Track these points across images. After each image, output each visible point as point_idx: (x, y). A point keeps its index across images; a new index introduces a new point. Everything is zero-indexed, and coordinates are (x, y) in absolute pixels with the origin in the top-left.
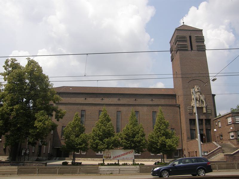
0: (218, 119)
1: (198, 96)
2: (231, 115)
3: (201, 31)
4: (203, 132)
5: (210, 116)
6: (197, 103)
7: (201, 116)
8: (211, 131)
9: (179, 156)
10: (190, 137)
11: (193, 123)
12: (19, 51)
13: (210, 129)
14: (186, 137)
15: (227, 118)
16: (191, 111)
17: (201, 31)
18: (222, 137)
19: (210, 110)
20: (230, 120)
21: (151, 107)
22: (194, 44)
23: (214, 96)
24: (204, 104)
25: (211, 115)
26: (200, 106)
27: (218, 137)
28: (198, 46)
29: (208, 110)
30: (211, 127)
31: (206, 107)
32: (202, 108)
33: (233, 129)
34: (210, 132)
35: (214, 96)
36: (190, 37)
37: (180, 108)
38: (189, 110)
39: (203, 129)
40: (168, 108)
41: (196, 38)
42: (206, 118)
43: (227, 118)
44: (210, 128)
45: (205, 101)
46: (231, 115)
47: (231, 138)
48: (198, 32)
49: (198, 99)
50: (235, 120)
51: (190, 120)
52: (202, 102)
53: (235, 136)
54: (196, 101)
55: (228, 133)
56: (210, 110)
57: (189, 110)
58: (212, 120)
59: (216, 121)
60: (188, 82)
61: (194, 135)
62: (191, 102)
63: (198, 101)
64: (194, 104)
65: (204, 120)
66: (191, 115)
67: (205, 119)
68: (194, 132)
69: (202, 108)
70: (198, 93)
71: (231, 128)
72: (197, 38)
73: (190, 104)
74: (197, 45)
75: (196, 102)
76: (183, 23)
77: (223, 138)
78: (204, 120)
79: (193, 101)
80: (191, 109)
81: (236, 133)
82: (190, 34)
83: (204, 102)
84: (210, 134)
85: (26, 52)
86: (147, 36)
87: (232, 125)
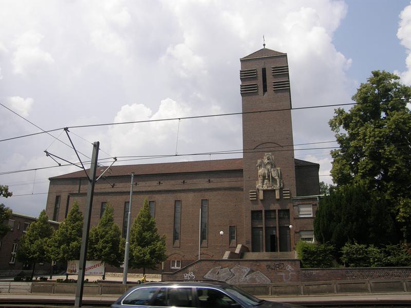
1: (266, 172)
3: (285, 56)
6: (265, 182)
7: (272, 205)
10: (251, 241)
12: (130, 105)
16: (288, 193)
17: (285, 56)
19: (289, 195)
21: (200, 193)
22: (270, 80)
26: (270, 188)
28: (277, 85)
32: (274, 191)
36: (264, 70)
38: (251, 195)
39: (276, 227)
40: (227, 192)
41: (273, 70)
42: (280, 209)
48: (278, 59)
50: (299, 212)
51: (253, 212)
52: (274, 180)
57: (251, 195)
63: (267, 179)
64: (259, 185)
65: (277, 211)
66: (255, 204)
68: (261, 232)
69: (274, 191)
72: (276, 69)
73: (255, 184)
74: (274, 83)
76: (264, 45)
78: (277, 211)
82: (264, 64)
83: (278, 181)
84: (288, 236)
85: (141, 104)
86: (340, 56)
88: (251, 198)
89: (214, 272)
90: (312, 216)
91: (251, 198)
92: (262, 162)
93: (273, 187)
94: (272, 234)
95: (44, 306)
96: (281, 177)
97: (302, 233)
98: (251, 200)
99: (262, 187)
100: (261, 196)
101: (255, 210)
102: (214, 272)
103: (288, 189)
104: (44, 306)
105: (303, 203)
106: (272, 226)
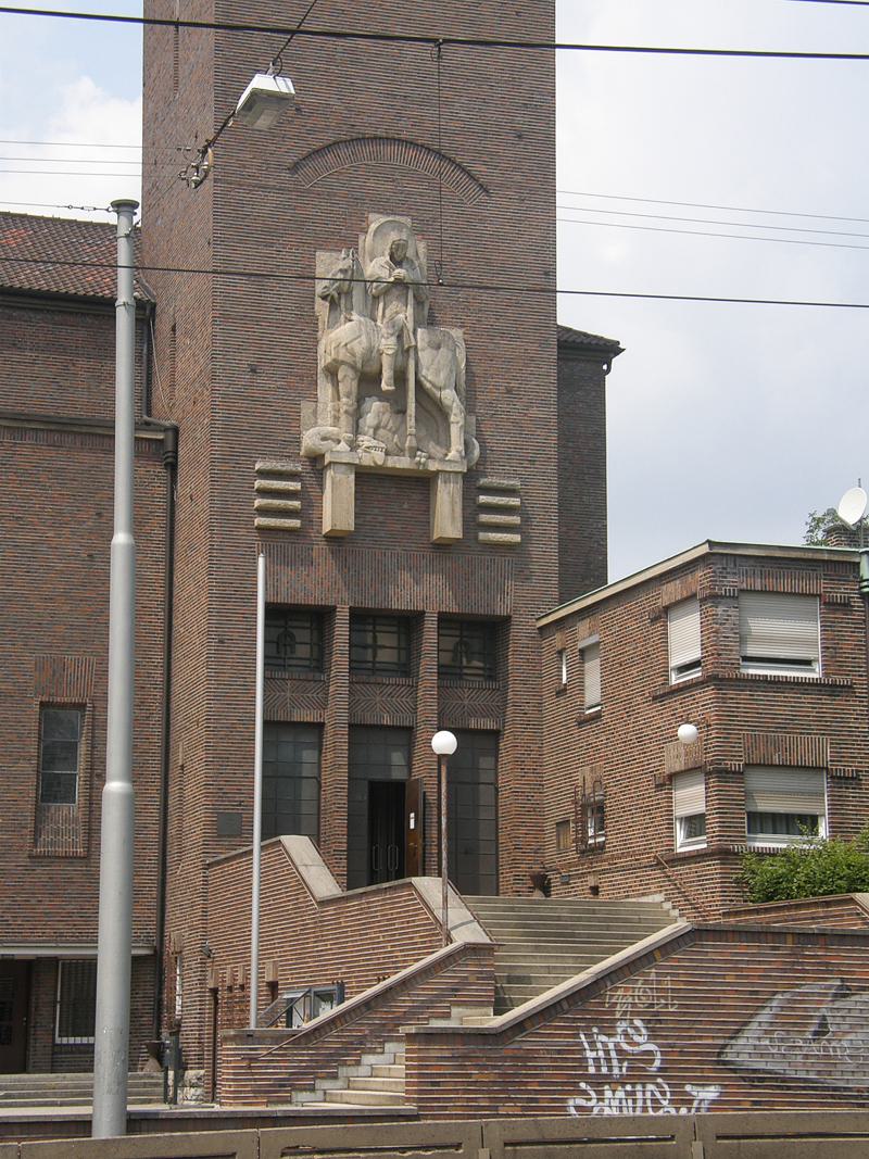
0: (583, 627)
1: (388, 345)
2: (699, 580)
4: (409, 765)
5: (510, 585)
6: (370, 420)
7: (406, 576)
8: (505, 758)
9: (58, 1040)
11: (303, 651)
13: (495, 735)
14: (200, 814)
15: (667, 609)
18: (601, 825)
19: (516, 520)
20: (686, 639)
23: (588, 357)
24: (448, 448)
25: (523, 575)
26: (403, 463)
27: (564, 823)
29: (484, 518)
30: (500, 711)
31: (470, 480)
32: (422, 484)
33: (702, 740)
34: (485, 762)
35: (588, 357)
37: (172, 467)
38: (264, 493)
42: (454, 609)
43: (663, 614)
44: (489, 724)
45: (469, 409)
46: (699, 580)
47: (682, 843)
49: (387, 374)
50: (743, 640)
52: (432, 410)
53: (713, 824)
54: (360, 400)
55: (659, 787)
56: (516, 520)
57: (264, 493)
58: (521, 633)
59: (558, 639)
60: (294, 168)
61: (307, 790)
62: (306, 408)
63: (383, 396)
64: (324, 425)
65: (431, 624)
67: (445, 620)
68: (308, 756)
69: (422, 484)
70: (394, 306)
71: (687, 731)
75: (357, 415)
77: (612, 839)
78: (431, 624)
79: (325, 390)
80: (295, 486)
81: (733, 788)
83: (457, 418)
84: (485, 795)
87: (697, 692)
88: (263, 512)
89: (791, 1021)
90: (815, 673)
91: (263, 512)
92: (353, 277)
93: (421, 457)
94: (379, 776)
95: (330, 1156)
96: (469, 393)
97: (757, 780)
98: (260, 529)
99: (354, 446)
100: (336, 507)
101: (370, 604)
102: (791, 1021)
103: (516, 483)
104: (330, 1156)
105: (771, 584)
106: (387, 721)
